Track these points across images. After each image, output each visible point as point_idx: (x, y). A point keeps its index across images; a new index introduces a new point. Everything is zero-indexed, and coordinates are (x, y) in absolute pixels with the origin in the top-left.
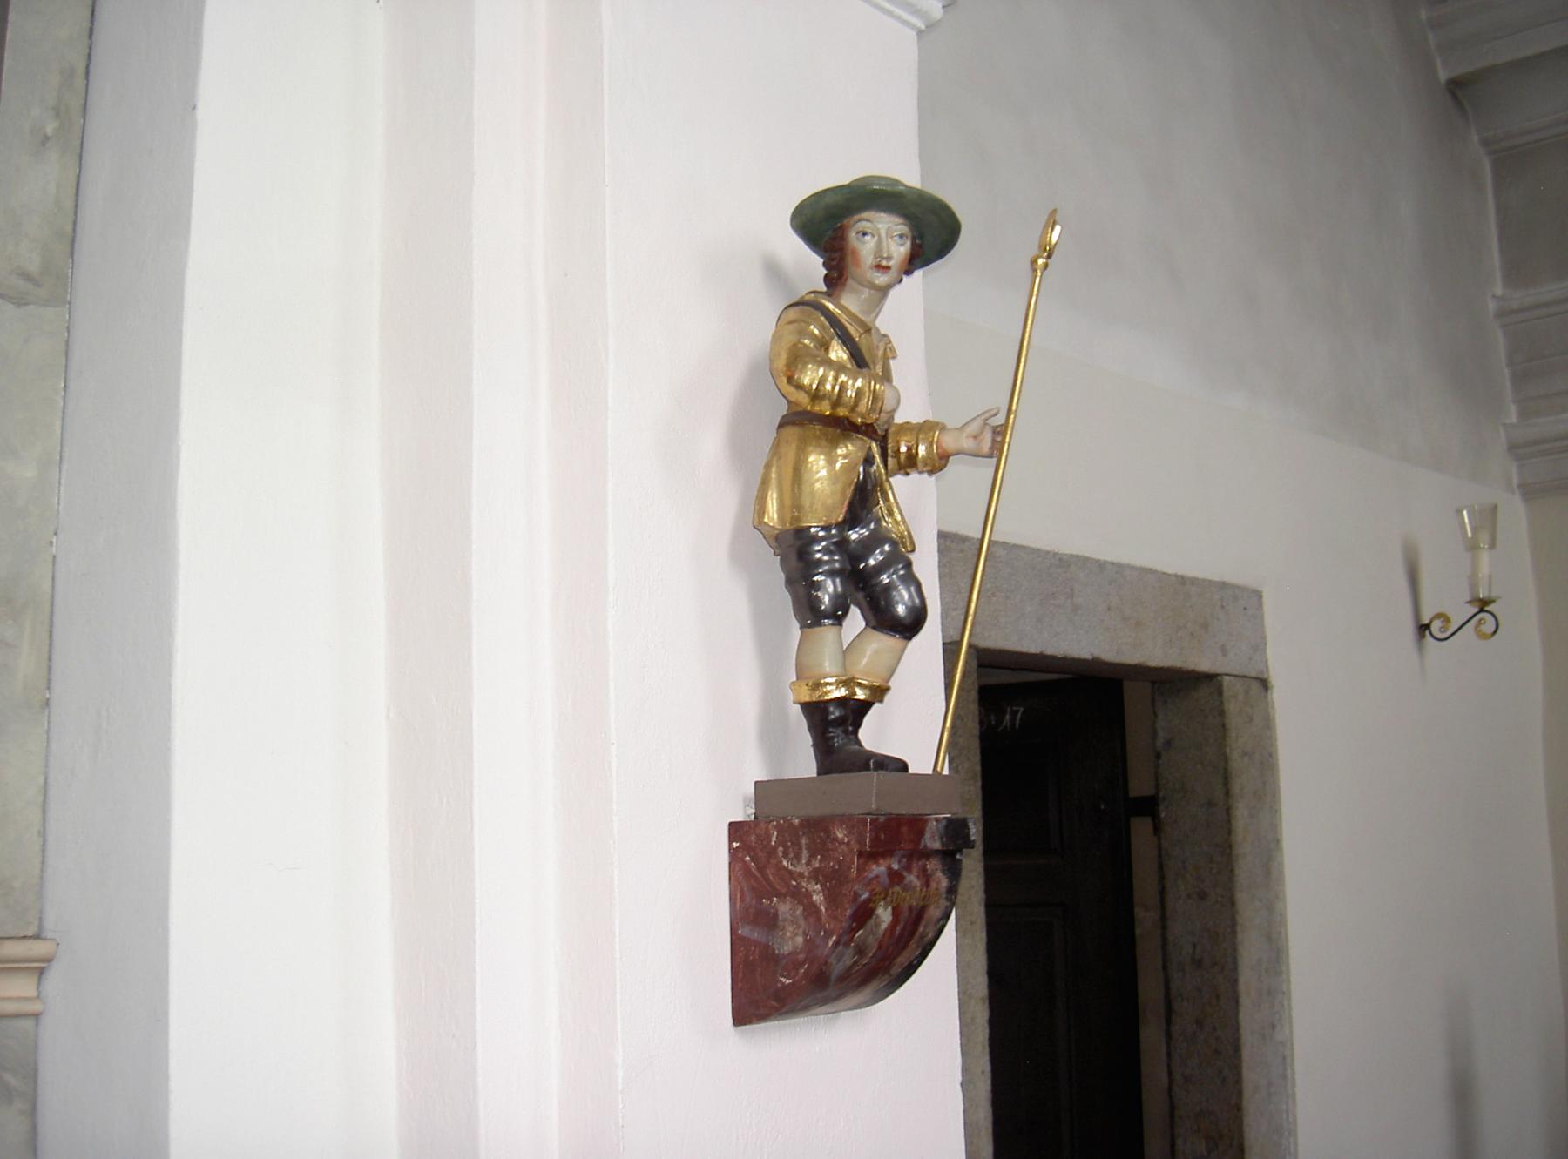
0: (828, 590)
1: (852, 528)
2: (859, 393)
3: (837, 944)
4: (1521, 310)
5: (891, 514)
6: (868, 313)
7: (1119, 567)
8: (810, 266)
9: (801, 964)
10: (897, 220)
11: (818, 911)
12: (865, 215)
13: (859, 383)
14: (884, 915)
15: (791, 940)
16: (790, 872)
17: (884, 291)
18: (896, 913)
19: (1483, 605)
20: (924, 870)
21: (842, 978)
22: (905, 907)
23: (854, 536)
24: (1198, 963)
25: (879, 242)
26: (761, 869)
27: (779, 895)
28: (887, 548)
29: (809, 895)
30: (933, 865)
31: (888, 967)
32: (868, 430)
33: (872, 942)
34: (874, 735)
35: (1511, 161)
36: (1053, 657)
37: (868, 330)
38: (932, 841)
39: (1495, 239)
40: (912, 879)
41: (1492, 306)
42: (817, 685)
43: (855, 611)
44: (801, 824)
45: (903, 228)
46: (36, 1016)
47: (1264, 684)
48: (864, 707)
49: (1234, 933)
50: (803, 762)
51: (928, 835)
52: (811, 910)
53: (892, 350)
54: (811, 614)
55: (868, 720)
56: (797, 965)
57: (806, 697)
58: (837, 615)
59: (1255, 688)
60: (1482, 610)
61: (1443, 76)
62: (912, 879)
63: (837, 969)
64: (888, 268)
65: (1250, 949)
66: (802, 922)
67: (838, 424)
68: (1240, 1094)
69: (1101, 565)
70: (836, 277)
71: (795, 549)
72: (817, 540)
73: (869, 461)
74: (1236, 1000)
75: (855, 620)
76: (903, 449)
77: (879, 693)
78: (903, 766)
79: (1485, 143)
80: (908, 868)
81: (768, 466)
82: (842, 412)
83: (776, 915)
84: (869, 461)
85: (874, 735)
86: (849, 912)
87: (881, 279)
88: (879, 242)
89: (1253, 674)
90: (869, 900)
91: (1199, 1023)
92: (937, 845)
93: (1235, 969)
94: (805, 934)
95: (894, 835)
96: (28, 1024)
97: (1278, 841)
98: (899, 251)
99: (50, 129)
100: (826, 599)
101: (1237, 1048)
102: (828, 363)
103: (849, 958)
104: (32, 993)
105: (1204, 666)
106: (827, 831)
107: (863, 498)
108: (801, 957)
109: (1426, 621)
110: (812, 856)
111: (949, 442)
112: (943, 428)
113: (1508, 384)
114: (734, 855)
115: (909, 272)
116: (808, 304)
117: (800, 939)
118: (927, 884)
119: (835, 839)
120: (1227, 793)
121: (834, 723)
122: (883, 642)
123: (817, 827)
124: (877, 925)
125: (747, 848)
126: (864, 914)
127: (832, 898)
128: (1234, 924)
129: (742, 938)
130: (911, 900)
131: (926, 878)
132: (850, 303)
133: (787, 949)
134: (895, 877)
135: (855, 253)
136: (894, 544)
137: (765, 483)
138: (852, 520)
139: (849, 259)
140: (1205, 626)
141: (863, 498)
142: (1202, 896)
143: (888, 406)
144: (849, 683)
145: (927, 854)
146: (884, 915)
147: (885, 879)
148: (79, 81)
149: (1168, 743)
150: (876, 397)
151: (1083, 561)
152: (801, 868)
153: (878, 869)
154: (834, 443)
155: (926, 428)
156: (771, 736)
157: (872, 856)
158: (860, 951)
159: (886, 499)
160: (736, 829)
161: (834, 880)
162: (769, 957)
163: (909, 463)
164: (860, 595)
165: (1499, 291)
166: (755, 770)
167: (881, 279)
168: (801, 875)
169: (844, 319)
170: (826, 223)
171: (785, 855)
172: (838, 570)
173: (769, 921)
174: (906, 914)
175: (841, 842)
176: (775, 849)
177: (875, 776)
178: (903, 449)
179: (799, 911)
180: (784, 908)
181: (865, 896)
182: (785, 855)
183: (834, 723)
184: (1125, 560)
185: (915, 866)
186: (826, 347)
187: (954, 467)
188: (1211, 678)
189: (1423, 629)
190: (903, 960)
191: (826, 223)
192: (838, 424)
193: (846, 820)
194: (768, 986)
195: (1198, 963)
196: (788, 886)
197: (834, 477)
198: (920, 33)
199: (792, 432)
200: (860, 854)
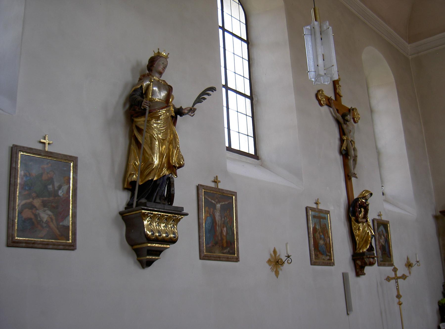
19: (418, 262)
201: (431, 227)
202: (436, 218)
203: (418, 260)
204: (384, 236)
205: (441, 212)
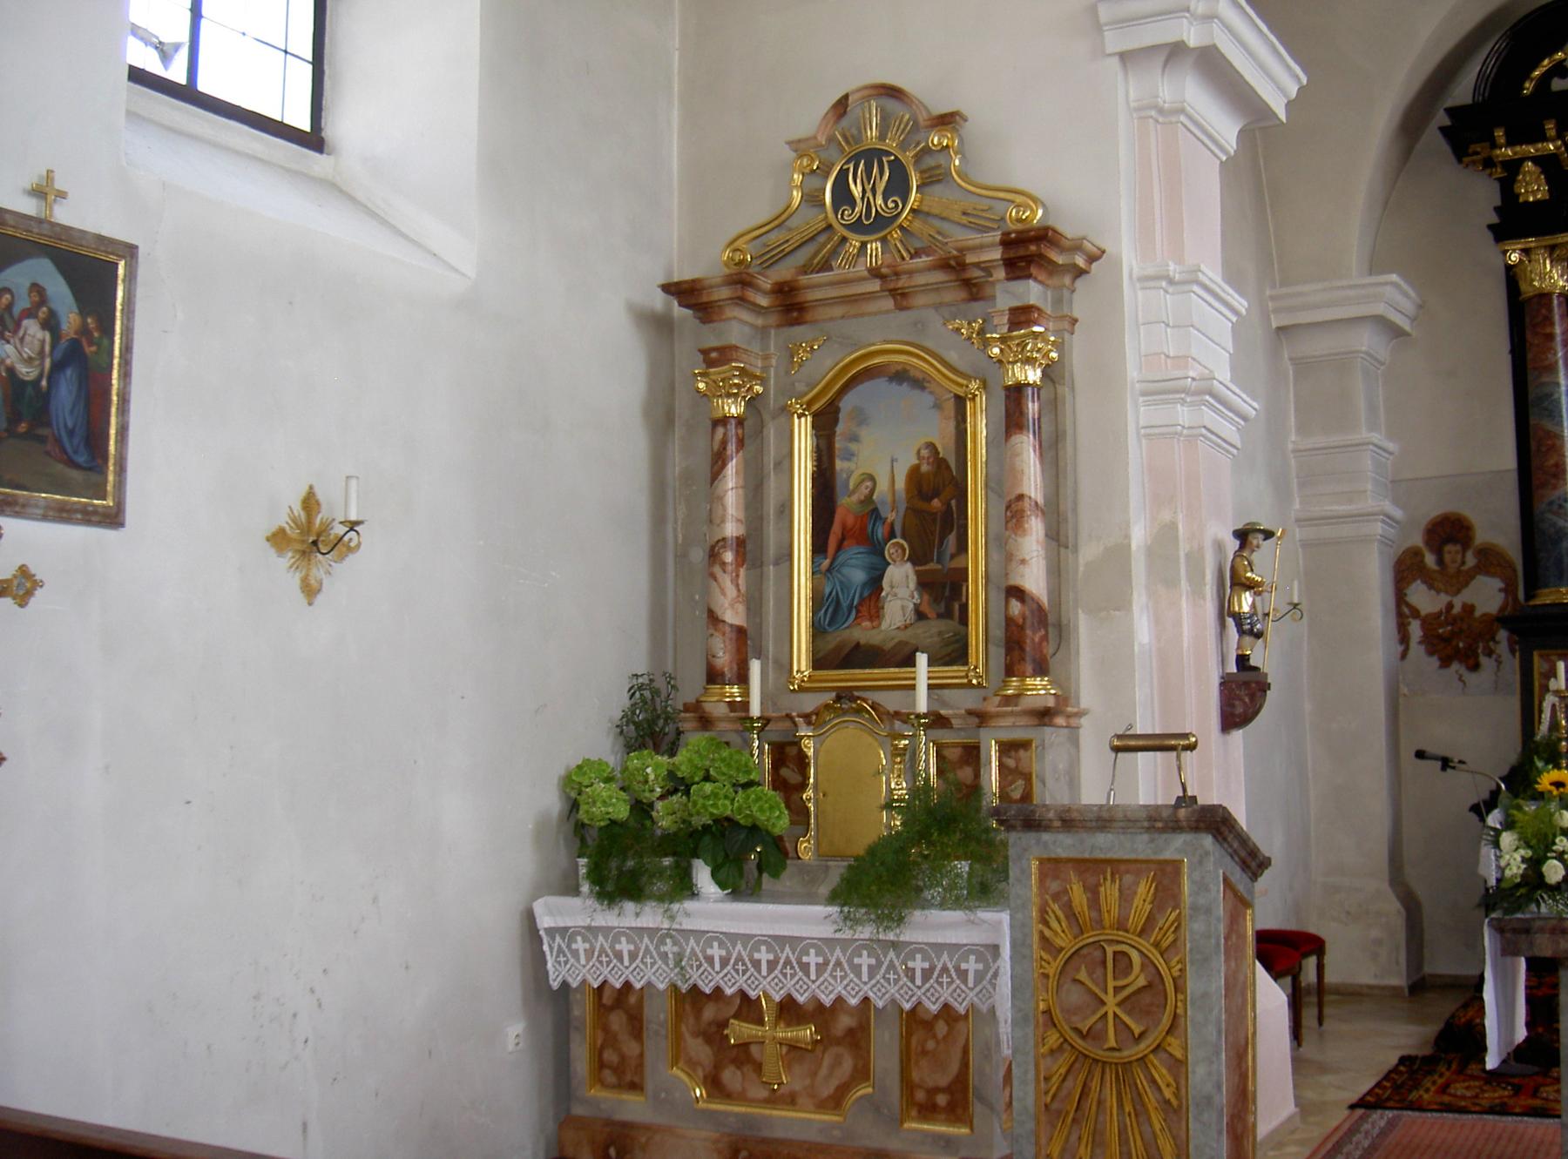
19: (1295, 606)
35: (1304, 367)
41: (1290, 446)
50: (1232, 668)
61: (1274, 325)
162: (1233, 715)
173: (1233, 706)
191: (1243, 535)
201: (602, 373)
202: (657, 326)
203: (353, 517)
204: (51, 324)
205: (668, 288)
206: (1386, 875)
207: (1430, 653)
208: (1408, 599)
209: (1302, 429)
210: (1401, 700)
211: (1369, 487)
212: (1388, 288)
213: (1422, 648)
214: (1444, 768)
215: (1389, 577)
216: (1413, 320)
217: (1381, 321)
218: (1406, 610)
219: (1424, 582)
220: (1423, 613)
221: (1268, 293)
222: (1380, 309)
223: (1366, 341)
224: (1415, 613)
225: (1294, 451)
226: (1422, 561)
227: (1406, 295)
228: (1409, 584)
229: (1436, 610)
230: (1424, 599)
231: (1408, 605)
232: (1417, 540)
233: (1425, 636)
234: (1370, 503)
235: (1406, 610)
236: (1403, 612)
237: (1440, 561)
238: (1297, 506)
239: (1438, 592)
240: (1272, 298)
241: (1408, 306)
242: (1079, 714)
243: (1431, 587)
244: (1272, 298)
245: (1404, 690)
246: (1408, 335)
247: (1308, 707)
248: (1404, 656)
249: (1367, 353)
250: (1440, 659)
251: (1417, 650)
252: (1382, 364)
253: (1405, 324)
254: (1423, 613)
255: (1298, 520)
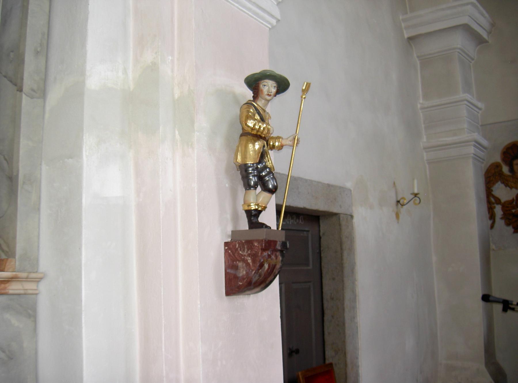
0: (253, 180)
1: (259, 164)
2: (264, 128)
3: (255, 273)
4: (428, 108)
5: (269, 161)
6: (264, 106)
7: (311, 181)
8: (249, 94)
9: (245, 279)
10: (274, 82)
11: (250, 265)
12: (265, 81)
13: (265, 125)
14: (266, 266)
15: (242, 272)
16: (242, 255)
17: (268, 101)
18: (269, 266)
19: (416, 195)
20: (276, 254)
21: (255, 283)
22: (271, 264)
23: (259, 166)
24: (332, 299)
25: (269, 88)
26: (234, 254)
27: (239, 261)
28: (268, 170)
29: (247, 260)
30: (278, 254)
31: (263, 283)
32: (264, 139)
33: (263, 273)
34: (262, 219)
35: (426, 62)
36: (293, 207)
37: (264, 111)
38: (279, 247)
39: (420, 86)
40: (273, 257)
41: (419, 106)
42: (249, 206)
43: (259, 186)
44: (245, 242)
45: (275, 85)
46: (37, 294)
47: (352, 217)
48: (260, 212)
49: (343, 290)
50: (244, 225)
51: (277, 245)
52: (248, 264)
53: (270, 117)
54: (248, 186)
55: (261, 215)
56: (244, 279)
57: (247, 208)
58: (255, 187)
59: (349, 217)
60: (415, 196)
61: (406, 36)
62: (273, 257)
63: (254, 280)
64: (270, 95)
65: (348, 295)
66: (245, 268)
67: (257, 136)
68: (345, 337)
69: (306, 180)
70: (256, 97)
71: (244, 169)
72: (250, 167)
73: (264, 146)
74: (344, 309)
75: (259, 189)
76: (271, 144)
77: (265, 208)
78: (270, 228)
79: (418, 57)
80: (272, 254)
81: (238, 147)
82: (259, 133)
83: (238, 266)
84: (264, 146)
85: (262, 219)
86: (258, 265)
87: (268, 98)
88: (269, 88)
89: (349, 214)
90: (263, 262)
91: (333, 317)
92: (279, 248)
93: (343, 300)
94: (246, 271)
95: (269, 245)
96: (34, 296)
97: (355, 263)
98: (274, 90)
99: (39, 49)
100: (252, 183)
101: (344, 324)
102: (255, 120)
103: (257, 278)
104: (35, 288)
105: (335, 210)
106: (252, 243)
107: (263, 155)
108: (245, 277)
109: (399, 200)
110: (248, 250)
111: (284, 142)
112: (282, 139)
113: (423, 129)
114: (226, 251)
115: (275, 96)
116: (249, 104)
117: (244, 272)
118: (276, 258)
119: (254, 246)
120: (341, 249)
121: (252, 215)
122: (266, 194)
123: (249, 243)
124: (265, 268)
125: (229, 248)
126: (262, 265)
127: (254, 261)
128: (343, 286)
129: (228, 273)
130: (273, 263)
131: (276, 257)
132: (260, 103)
133: (241, 275)
134: (269, 256)
135: (262, 91)
136: (270, 169)
137: (237, 151)
138: (260, 162)
139: (260, 92)
140: (335, 199)
141: (263, 155)
142: (334, 279)
143: (271, 133)
144: (258, 205)
145: (276, 250)
146: (266, 266)
147: (267, 256)
148: (46, 36)
149: (324, 234)
150: (268, 130)
151: (301, 179)
152: (245, 253)
153: (265, 254)
154: (255, 141)
155: (278, 138)
156: (235, 218)
157: (263, 250)
158: (260, 276)
159: (268, 157)
160: (226, 244)
161: (254, 257)
162: (236, 277)
163: (273, 147)
164: (260, 182)
165: (421, 101)
166: (229, 229)
167: (268, 98)
168: (245, 255)
169: (259, 108)
170: (254, 83)
171: (240, 250)
172: (256, 176)
173: (236, 268)
174: (271, 266)
175: (256, 246)
176: (237, 249)
177: (265, 230)
178: (271, 144)
179: (244, 265)
180: (240, 264)
181: (262, 260)
182: (240, 250)
183: (252, 215)
184: (313, 179)
185: (274, 253)
186: (254, 115)
187: (284, 149)
188: (336, 214)
189: (398, 202)
190: (269, 279)
191: (254, 83)
192: (257, 136)
193: (257, 241)
194: (236, 285)
195: (332, 299)
196: (241, 258)
197: (255, 150)
198: (270, 29)
199: (244, 138)
200: (262, 249)
206: (483, 360)
207: (508, 224)
208: (493, 193)
209: (426, 97)
210: (492, 253)
211: (466, 126)
212: (469, 7)
213: (503, 222)
214: (505, 310)
215: (482, 181)
216: (489, 33)
217: (466, 28)
218: (493, 200)
219: (503, 183)
220: (503, 201)
221: (401, 18)
222: (465, 20)
223: (459, 41)
224: (498, 201)
225: (422, 108)
226: (501, 170)
227: (482, 15)
228: (494, 184)
229: (510, 198)
230: (503, 193)
231: (494, 197)
232: (497, 158)
233: (504, 214)
234: (465, 136)
235: (493, 200)
236: (491, 200)
237: (512, 170)
238: (425, 140)
239: (511, 188)
240: (404, 20)
241: (487, 26)
242: (38, 280)
243: (507, 185)
244: (404, 20)
245: (493, 246)
246: (486, 42)
247: (434, 258)
248: (492, 227)
249: (460, 49)
250: (514, 228)
251: (500, 223)
252: (473, 59)
253: (485, 35)
254: (503, 201)
255: (425, 148)
